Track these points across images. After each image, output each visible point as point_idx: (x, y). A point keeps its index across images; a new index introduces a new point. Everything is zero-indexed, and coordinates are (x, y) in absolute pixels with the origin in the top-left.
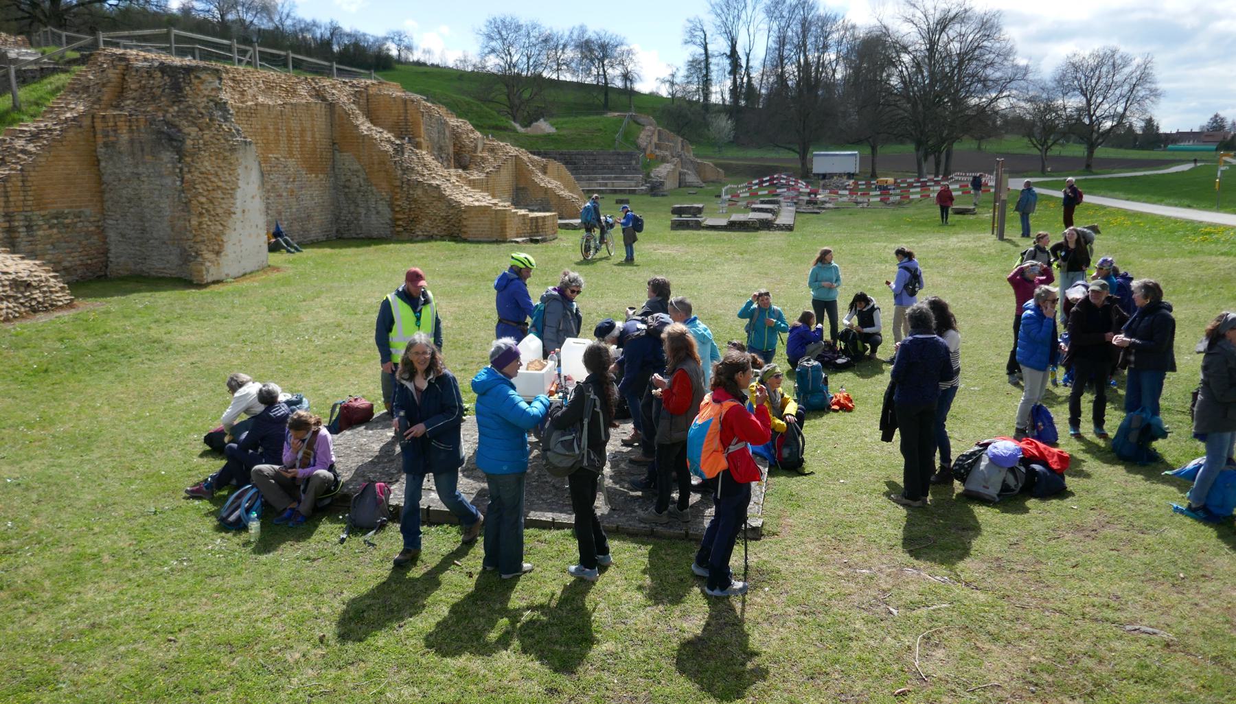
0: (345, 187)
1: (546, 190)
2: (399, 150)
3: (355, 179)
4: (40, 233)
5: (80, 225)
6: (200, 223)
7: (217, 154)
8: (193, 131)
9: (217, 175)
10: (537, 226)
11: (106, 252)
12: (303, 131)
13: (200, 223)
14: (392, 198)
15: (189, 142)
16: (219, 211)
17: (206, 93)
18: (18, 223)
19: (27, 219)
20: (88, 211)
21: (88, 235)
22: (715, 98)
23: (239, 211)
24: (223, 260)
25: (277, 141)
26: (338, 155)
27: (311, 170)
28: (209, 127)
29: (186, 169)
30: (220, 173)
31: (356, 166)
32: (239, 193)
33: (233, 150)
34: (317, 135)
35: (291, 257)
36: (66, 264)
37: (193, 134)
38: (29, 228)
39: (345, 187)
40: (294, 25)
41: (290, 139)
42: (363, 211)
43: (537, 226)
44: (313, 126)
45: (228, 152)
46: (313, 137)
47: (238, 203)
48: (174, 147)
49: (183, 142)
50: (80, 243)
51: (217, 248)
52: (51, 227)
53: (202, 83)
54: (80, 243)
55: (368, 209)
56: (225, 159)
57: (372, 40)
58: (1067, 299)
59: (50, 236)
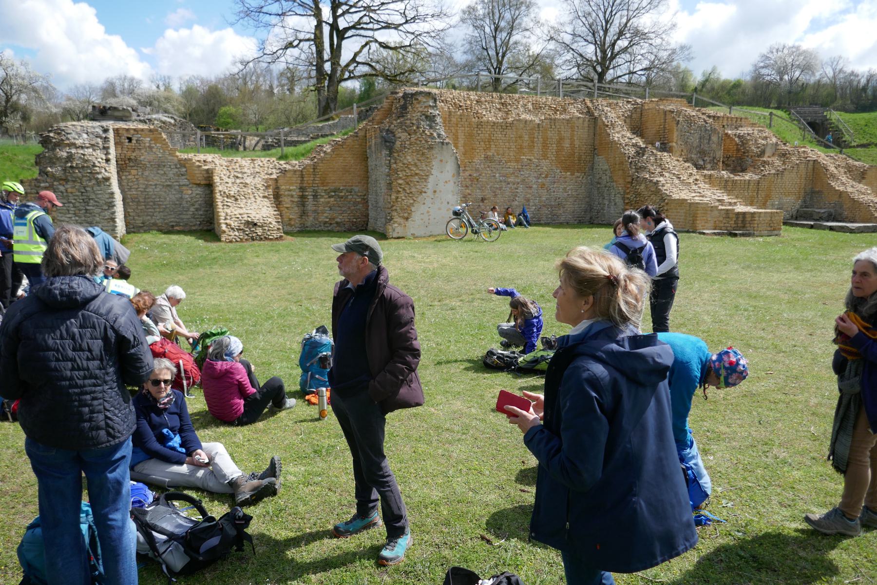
0: (598, 183)
1: (840, 194)
2: (641, 152)
3: (604, 177)
4: (322, 200)
5: (350, 197)
6: (397, 198)
7: (418, 151)
8: (404, 136)
9: (416, 165)
10: (743, 221)
11: (367, 216)
12: (561, 139)
13: (397, 198)
14: (624, 192)
15: (398, 143)
16: (413, 190)
17: (420, 109)
18: (309, 193)
19: (315, 191)
20: (356, 189)
21: (356, 203)
22: (533, 42)
23: (430, 193)
24: (409, 223)
25: (531, 147)
26: (596, 158)
27: (566, 169)
28: (415, 132)
29: (393, 161)
30: (419, 164)
31: (606, 167)
32: (431, 179)
33: (431, 148)
34: (577, 143)
35: (525, 229)
36: (338, 220)
37: (403, 137)
38: (315, 196)
39: (598, 183)
40: (844, 78)
41: (545, 145)
42: (607, 203)
43: (743, 221)
44: (572, 136)
45: (427, 149)
46: (572, 144)
47: (430, 186)
48: (387, 147)
49: (394, 143)
50: (349, 208)
51: (406, 215)
52: (330, 197)
53: (419, 103)
54: (349, 208)
55: (610, 202)
56: (423, 154)
57: (863, 81)
58: (13, 262)
59: (329, 202)
